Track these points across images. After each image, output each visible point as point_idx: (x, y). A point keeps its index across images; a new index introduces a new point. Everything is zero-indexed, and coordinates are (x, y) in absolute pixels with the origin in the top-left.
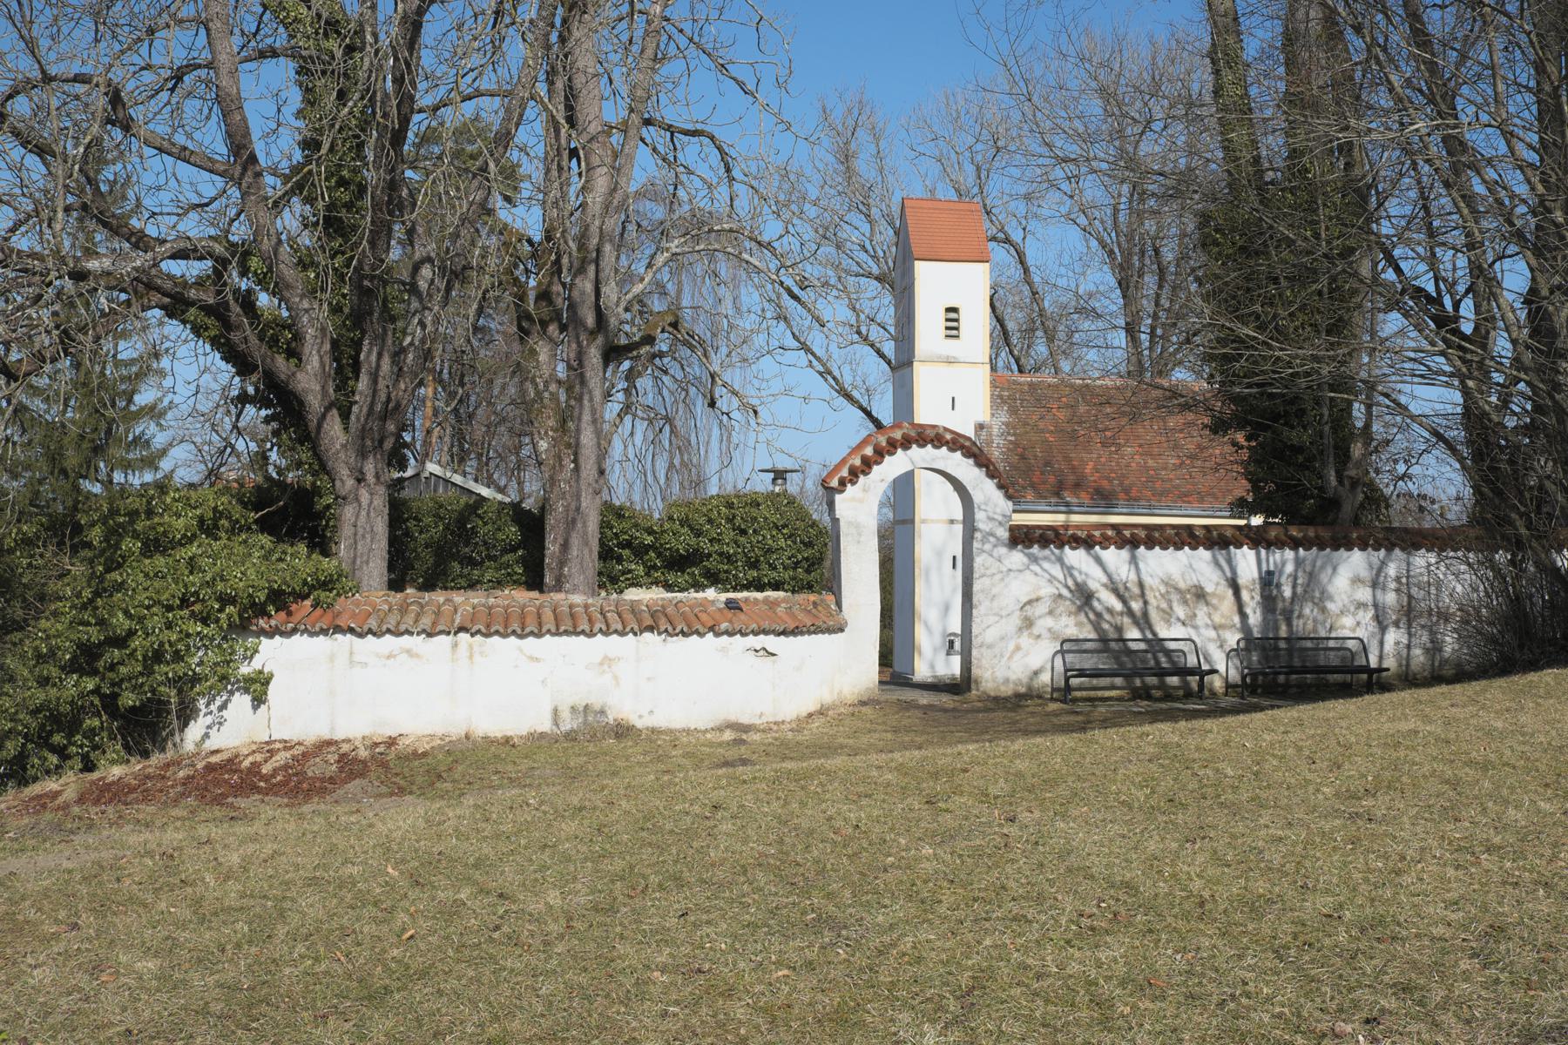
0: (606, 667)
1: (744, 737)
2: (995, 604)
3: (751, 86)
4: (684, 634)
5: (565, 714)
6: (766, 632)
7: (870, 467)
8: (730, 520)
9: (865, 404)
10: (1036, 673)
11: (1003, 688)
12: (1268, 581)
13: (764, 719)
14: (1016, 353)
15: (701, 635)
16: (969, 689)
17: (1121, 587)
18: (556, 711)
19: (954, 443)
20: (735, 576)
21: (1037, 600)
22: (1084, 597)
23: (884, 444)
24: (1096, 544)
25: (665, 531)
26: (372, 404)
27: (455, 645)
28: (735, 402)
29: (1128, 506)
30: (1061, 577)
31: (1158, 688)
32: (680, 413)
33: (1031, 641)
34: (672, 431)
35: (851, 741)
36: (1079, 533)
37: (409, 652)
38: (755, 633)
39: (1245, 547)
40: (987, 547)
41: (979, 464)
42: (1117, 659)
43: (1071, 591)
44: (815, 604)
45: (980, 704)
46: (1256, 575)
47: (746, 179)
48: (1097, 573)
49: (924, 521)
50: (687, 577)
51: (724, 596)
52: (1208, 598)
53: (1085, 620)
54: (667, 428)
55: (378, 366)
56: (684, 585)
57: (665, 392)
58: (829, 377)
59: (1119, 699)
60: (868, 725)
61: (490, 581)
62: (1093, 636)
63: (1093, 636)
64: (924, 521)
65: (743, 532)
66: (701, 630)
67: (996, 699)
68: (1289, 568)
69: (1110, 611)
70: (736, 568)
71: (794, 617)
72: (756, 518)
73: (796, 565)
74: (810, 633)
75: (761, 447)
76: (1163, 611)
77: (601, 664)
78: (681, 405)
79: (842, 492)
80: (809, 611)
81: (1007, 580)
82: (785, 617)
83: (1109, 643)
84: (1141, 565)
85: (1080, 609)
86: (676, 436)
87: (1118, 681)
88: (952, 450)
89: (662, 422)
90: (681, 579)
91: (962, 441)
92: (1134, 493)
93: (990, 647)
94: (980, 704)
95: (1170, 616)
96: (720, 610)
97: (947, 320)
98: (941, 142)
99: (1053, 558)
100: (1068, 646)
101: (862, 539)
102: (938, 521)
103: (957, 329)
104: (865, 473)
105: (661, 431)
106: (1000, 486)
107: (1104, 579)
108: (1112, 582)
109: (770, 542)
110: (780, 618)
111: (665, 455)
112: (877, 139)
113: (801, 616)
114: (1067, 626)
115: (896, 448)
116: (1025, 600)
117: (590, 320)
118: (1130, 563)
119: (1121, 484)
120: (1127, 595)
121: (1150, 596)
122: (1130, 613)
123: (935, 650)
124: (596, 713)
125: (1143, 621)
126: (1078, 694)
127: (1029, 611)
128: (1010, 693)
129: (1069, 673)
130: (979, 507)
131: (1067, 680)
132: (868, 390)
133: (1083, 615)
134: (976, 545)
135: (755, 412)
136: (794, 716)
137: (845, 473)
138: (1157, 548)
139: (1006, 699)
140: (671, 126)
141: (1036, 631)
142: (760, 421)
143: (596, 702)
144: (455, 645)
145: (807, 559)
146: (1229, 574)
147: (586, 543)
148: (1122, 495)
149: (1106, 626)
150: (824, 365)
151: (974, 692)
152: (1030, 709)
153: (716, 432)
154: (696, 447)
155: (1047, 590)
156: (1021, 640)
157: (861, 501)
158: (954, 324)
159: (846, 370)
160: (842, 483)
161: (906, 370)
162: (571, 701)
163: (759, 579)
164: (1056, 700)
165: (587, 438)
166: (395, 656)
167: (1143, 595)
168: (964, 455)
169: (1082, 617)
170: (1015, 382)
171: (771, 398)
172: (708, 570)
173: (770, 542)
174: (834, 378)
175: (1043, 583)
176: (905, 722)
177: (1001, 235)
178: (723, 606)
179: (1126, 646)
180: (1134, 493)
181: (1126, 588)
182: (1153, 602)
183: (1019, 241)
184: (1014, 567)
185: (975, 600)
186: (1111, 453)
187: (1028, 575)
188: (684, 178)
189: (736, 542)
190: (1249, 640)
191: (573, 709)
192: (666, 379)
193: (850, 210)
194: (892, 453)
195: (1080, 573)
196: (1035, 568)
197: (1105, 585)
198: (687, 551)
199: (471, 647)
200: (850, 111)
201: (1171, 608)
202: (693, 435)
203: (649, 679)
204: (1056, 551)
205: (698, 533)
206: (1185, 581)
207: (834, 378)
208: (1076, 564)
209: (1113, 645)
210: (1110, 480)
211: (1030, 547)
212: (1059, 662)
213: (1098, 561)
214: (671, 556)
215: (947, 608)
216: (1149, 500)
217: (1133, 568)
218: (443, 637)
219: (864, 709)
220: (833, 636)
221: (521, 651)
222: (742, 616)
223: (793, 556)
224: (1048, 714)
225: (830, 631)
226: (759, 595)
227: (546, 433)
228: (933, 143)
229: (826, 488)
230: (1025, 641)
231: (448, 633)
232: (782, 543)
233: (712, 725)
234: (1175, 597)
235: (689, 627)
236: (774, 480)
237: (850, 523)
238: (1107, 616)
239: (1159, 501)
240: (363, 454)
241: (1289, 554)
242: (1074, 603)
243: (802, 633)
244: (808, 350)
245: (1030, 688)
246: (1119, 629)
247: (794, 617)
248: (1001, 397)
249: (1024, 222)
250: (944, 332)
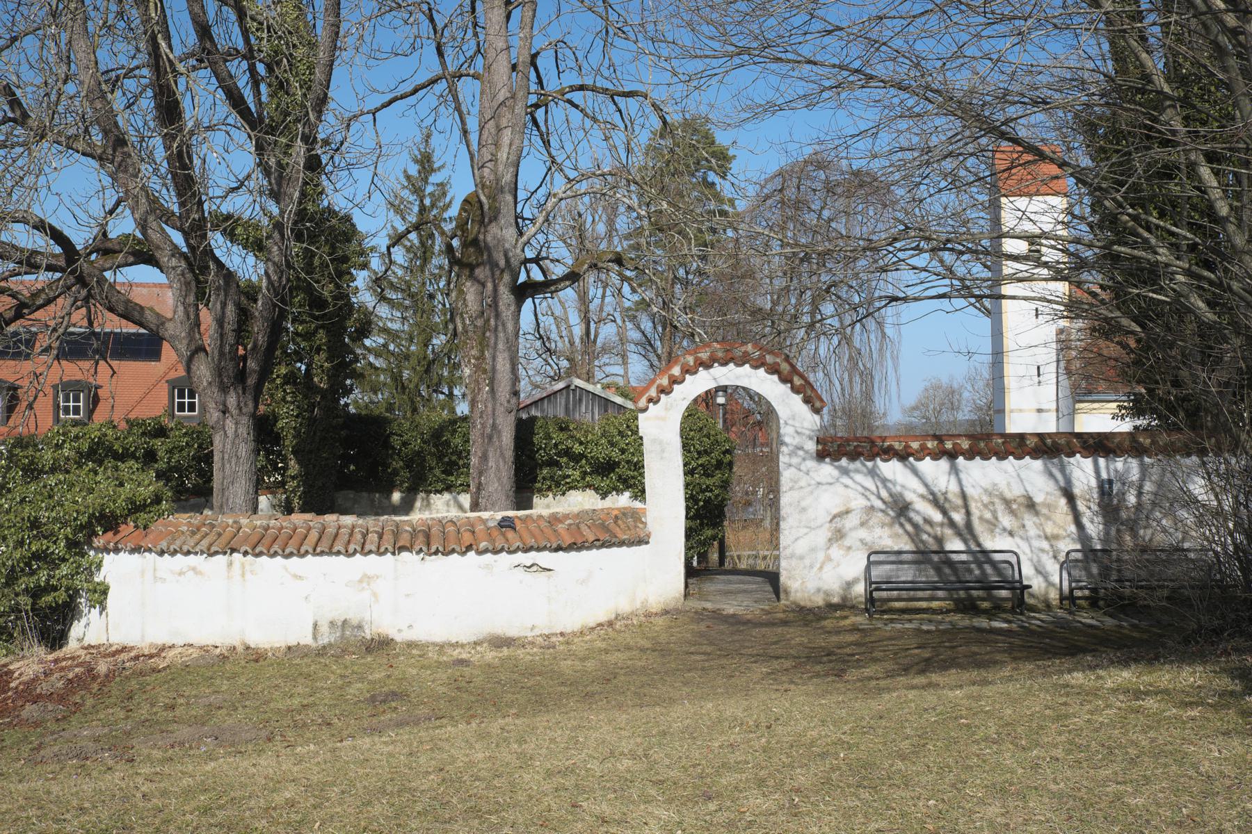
0: (364, 584)
5: (324, 628)
12: (1105, 488)
13: (537, 632)
17: (942, 501)
18: (315, 625)
21: (847, 512)
22: (901, 509)
26: (222, 346)
27: (230, 564)
30: (873, 488)
33: (842, 552)
37: (194, 569)
39: (1078, 455)
43: (884, 502)
46: (1094, 483)
48: (914, 483)
49: (1012, 411)
52: (1038, 508)
55: (223, 313)
61: (461, 485)
62: (909, 547)
64: (1012, 411)
68: (1135, 475)
69: (928, 521)
76: (988, 521)
77: (361, 581)
83: (922, 556)
84: (962, 476)
93: (801, 558)
100: (875, 556)
102: (1030, 410)
107: (922, 490)
108: (932, 493)
116: (835, 511)
117: (502, 263)
120: (947, 505)
121: (973, 507)
122: (952, 524)
124: (353, 627)
125: (967, 532)
127: (838, 523)
130: (786, 423)
141: (847, 542)
143: (354, 618)
144: (230, 564)
146: (1062, 483)
147: (502, 454)
149: (925, 537)
155: (859, 503)
162: (331, 616)
165: (503, 364)
166: (184, 573)
167: (966, 506)
172: (620, 477)
184: (824, 481)
187: (839, 488)
190: (1088, 552)
191: (332, 624)
196: (846, 480)
197: (922, 497)
199: (243, 566)
201: (996, 518)
203: (408, 595)
206: (1010, 490)
211: (839, 460)
218: (220, 557)
221: (286, 570)
225: (631, 543)
227: (469, 361)
231: (225, 553)
234: (1000, 507)
237: (654, 441)
240: (224, 389)
241: (1134, 464)
246: (940, 540)
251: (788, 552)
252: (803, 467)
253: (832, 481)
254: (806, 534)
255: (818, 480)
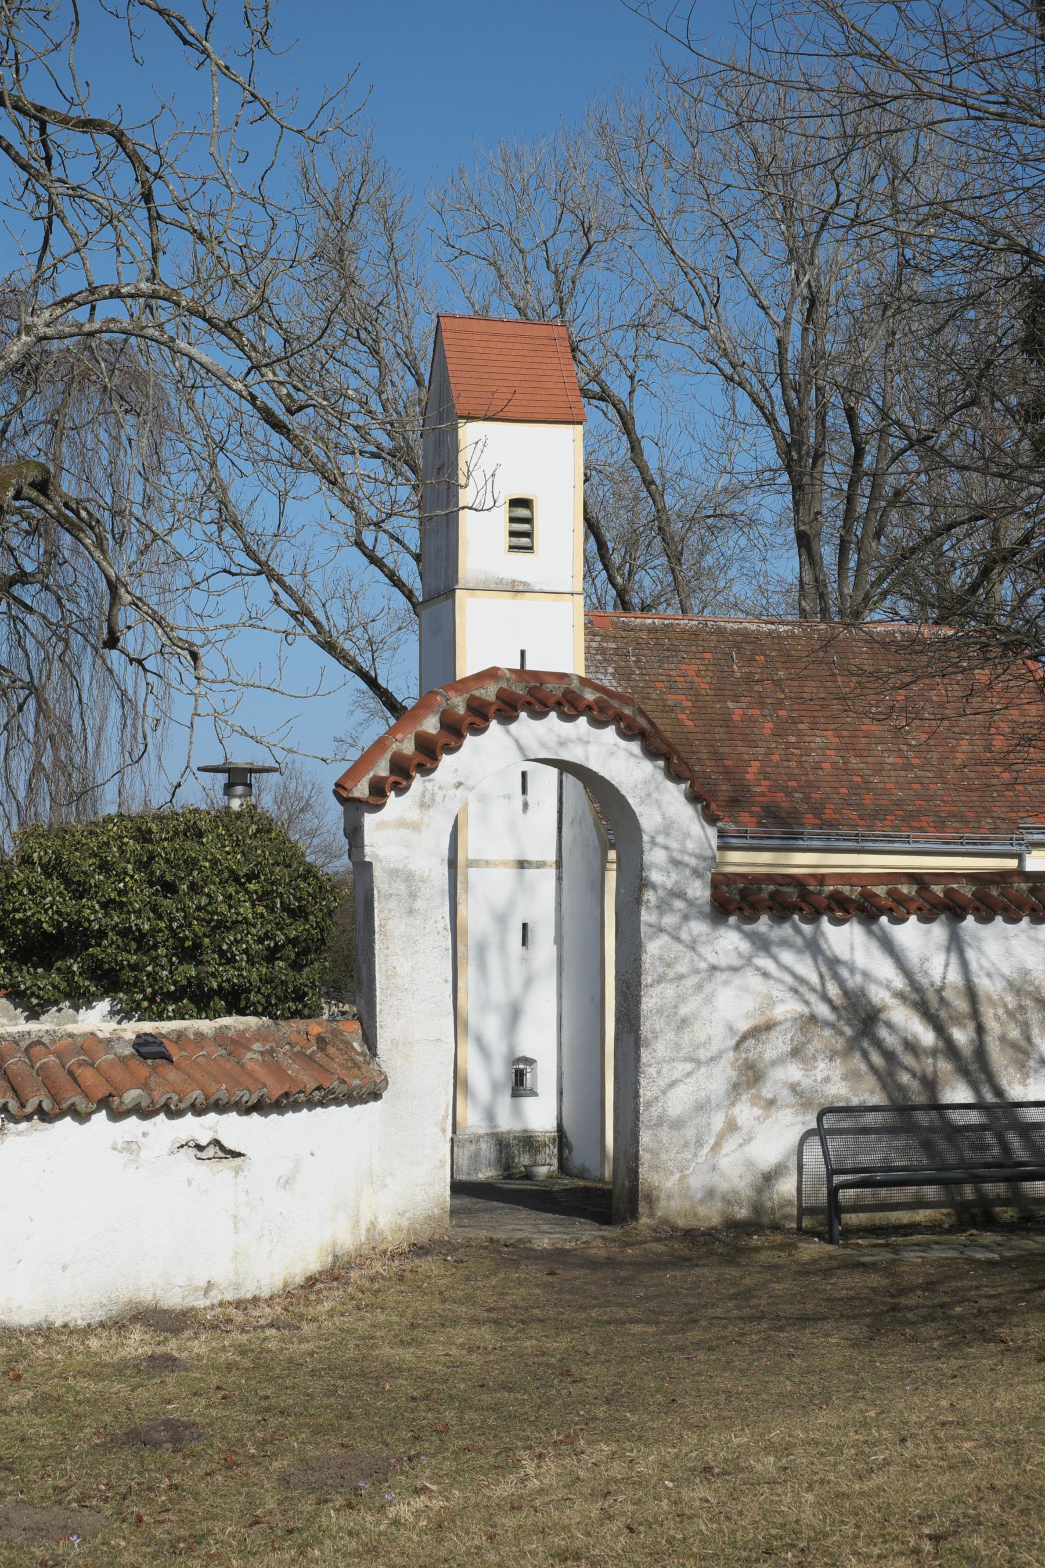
1: (172, 1347)
2: (686, 1037)
3: (195, 27)
4: (46, 1116)
6: (220, 1107)
7: (435, 759)
8: (144, 865)
9: (366, 666)
10: (769, 1178)
11: (702, 1211)
13: (215, 1297)
14: (619, 580)
15: (82, 1117)
16: (634, 1214)
19: (602, 710)
20: (152, 976)
23: (461, 710)
24: (881, 912)
25: (14, 886)
28: (154, 636)
29: (818, 837)
30: (814, 979)
31: (1006, 1202)
32: (54, 678)
33: (757, 1111)
34: (39, 710)
35: (407, 1355)
36: (846, 890)
38: (199, 1110)
40: (669, 920)
41: (651, 753)
42: (927, 1146)
43: (834, 1008)
44: (321, 1040)
45: (659, 1248)
47: (181, 217)
48: (884, 969)
50: (55, 977)
51: (132, 1029)
53: (863, 1067)
54: (32, 703)
56: (50, 993)
57: (30, 643)
58: (307, 622)
59: (933, 1228)
60: (437, 1306)
63: (877, 1099)
65: (169, 889)
66: (82, 1105)
67: (689, 1234)
69: (911, 1046)
70: (154, 960)
71: (279, 1072)
72: (195, 861)
73: (272, 955)
74: (311, 1104)
75: (204, 726)
76: (1014, 1045)
78: (56, 665)
79: (377, 807)
80: (310, 1058)
81: (708, 989)
82: (261, 1073)
84: (971, 954)
85: (852, 1045)
86: (47, 718)
87: (931, 1192)
88: (598, 723)
89: (22, 694)
90: (46, 980)
91: (615, 703)
92: (829, 814)
93: (678, 1124)
94: (659, 1248)
95: (1026, 1054)
96: (123, 1060)
97: (513, 520)
98: (495, 234)
99: (799, 941)
101: (419, 904)
102: (505, 863)
103: (529, 535)
104: (426, 770)
105: (20, 708)
106: (693, 798)
107: (899, 983)
109: (223, 908)
110: (250, 1074)
111: (28, 750)
112: (389, 229)
113: (294, 1069)
114: (827, 1080)
115: (486, 719)
116: (744, 1026)
118: (948, 950)
119: (807, 799)
120: (943, 1014)
122: (951, 1049)
123: (495, 1088)
126: (852, 1219)
127: (753, 1050)
128: (716, 1220)
129: (837, 1179)
130: (653, 842)
131: (833, 1192)
132: (370, 642)
133: (858, 1055)
134: (647, 916)
135: (195, 656)
136: (278, 1284)
137: (382, 769)
138: (999, 919)
139: (711, 1234)
140: (42, 109)
142: (203, 673)
145: (294, 942)
148: (809, 818)
149: (905, 1078)
150: (297, 601)
151: (644, 1220)
152: (764, 1257)
153: (115, 710)
154: (80, 736)
155: (788, 1008)
156: (736, 1111)
157: (416, 827)
158: (524, 527)
159: (335, 608)
160: (379, 791)
161: (443, 605)
163: (200, 982)
164: (811, 1233)
167: (975, 1014)
168: (623, 734)
169: (857, 1062)
170: (626, 627)
171: (223, 633)
172: (100, 964)
173: (223, 908)
174: (316, 623)
175: (777, 991)
176: (517, 1295)
177: (595, 387)
178: (129, 1051)
179: (942, 1117)
180: (829, 814)
181: (942, 1001)
182: (993, 1026)
183: (624, 397)
184: (722, 961)
185: (646, 1028)
186: (789, 746)
188: (63, 204)
189: (154, 910)
192: (30, 619)
193: (344, 342)
194: (478, 730)
195: (852, 970)
196: (764, 962)
197: (900, 995)
198: (58, 925)
200: (347, 176)
201: (1028, 1039)
202: (76, 715)
204: (807, 928)
205: (80, 891)
207: (316, 623)
208: (844, 954)
209: (923, 1119)
210: (789, 794)
211: (753, 919)
212: (813, 1154)
213: (888, 946)
214: (25, 933)
215: (514, 1015)
216: (855, 826)
217: (954, 959)
219: (427, 1265)
220: (358, 1108)
222: (171, 1074)
223: (267, 936)
224: (805, 1271)
225: (353, 1098)
226: (206, 1026)
228: (483, 235)
229: (343, 800)
230: (745, 1112)
232: (246, 910)
233: (99, 1316)
235: (55, 1099)
236: (228, 788)
237: (394, 874)
238: (908, 1060)
239: (871, 828)
242: (841, 1033)
243: (296, 1107)
244: (273, 576)
245: (757, 1208)
246: (930, 1084)
247: (279, 1072)
248: (601, 650)
249: (631, 366)
250: (505, 540)
251: (655, 1111)
252: (684, 935)
253: (736, 962)
254: (689, 1074)
255: (712, 959)
